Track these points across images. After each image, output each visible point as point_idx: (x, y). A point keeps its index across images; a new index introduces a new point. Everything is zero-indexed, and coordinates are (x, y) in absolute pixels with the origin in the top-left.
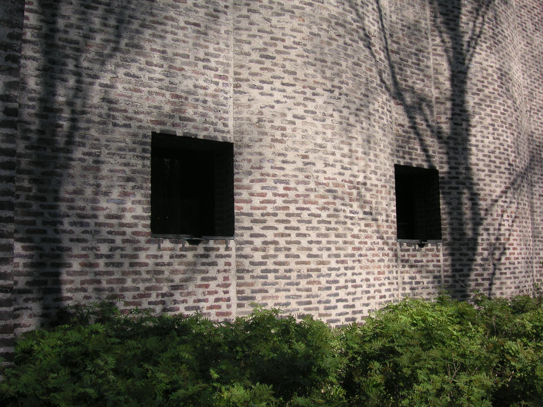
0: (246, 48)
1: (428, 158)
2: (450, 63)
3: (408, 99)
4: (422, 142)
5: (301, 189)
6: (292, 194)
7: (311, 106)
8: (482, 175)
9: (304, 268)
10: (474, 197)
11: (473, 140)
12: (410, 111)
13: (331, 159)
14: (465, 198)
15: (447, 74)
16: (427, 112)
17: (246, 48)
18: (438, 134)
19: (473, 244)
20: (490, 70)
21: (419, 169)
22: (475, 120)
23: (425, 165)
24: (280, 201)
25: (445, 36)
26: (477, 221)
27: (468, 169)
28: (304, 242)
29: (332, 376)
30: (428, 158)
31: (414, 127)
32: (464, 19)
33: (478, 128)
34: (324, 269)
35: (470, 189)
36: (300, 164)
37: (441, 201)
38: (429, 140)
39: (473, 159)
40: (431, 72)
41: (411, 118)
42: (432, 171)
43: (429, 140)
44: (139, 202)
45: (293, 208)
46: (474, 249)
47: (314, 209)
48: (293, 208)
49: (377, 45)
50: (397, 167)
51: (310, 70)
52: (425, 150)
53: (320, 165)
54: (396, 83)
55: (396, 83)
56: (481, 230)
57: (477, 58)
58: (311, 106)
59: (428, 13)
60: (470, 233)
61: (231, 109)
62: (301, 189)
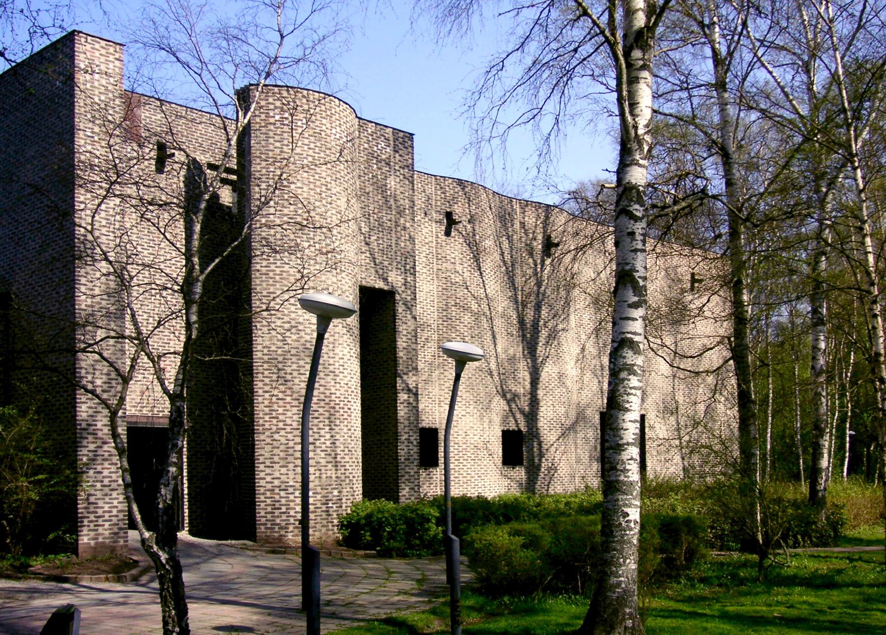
0: (443, 387)
1: (517, 425)
2: (530, 374)
3: (508, 396)
4: (514, 417)
5: (464, 446)
6: (460, 449)
7: (468, 410)
8: (545, 432)
9: (465, 480)
10: (540, 444)
11: (542, 414)
12: (509, 402)
13: (476, 433)
14: (535, 444)
15: (529, 380)
16: (518, 402)
17: (443, 387)
18: (522, 412)
19: (538, 468)
20: (553, 375)
21: (513, 431)
22: (541, 404)
23: (516, 429)
24: (456, 452)
25: (529, 360)
26: (541, 455)
27: (537, 429)
28: (465, 468)
29: (663, 136)
30: (517, 425)
31: (511, 411)
32: (539, 349)
33: (545, 407)
34: (473, 480)
35: (539, 439)
36: (464, 435)
37: (125, 440)
38: (518, 416)
39: (540, 424)
40: (521, 380)
41: (510, 406)
42: (520, 431)
43: (518, 416)
44: (262, 471)
45: (461, 454)
46: (539, 470)
47: (469, 454)
48: (461, 454)
49: (495, 374)
50: (503, 431)
51: (468, 394)
52: (516, 421)
53: (472, 436)
54: (503, 390)
55: (503, 390)
56: (543, 460)
57: (546, 369)
58: (468, 410)
59: (520, 349)
60: (536, 461)
61: (437, 414)
62: (464, 446)
